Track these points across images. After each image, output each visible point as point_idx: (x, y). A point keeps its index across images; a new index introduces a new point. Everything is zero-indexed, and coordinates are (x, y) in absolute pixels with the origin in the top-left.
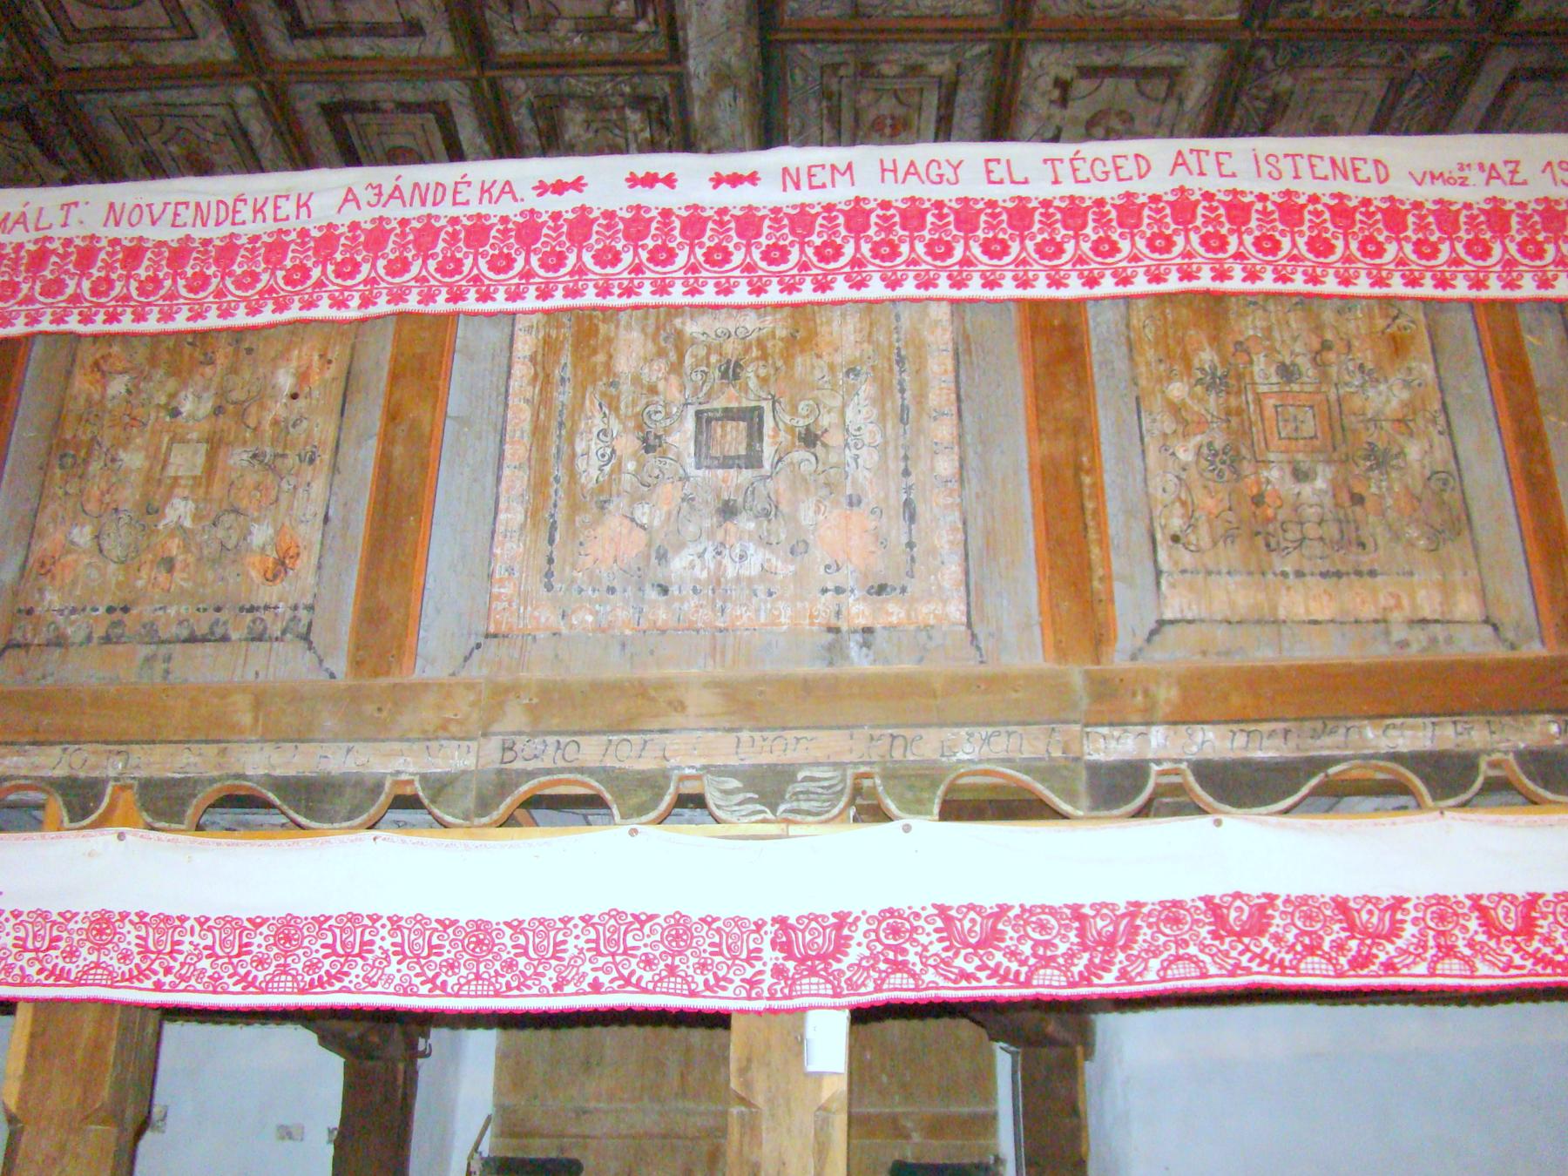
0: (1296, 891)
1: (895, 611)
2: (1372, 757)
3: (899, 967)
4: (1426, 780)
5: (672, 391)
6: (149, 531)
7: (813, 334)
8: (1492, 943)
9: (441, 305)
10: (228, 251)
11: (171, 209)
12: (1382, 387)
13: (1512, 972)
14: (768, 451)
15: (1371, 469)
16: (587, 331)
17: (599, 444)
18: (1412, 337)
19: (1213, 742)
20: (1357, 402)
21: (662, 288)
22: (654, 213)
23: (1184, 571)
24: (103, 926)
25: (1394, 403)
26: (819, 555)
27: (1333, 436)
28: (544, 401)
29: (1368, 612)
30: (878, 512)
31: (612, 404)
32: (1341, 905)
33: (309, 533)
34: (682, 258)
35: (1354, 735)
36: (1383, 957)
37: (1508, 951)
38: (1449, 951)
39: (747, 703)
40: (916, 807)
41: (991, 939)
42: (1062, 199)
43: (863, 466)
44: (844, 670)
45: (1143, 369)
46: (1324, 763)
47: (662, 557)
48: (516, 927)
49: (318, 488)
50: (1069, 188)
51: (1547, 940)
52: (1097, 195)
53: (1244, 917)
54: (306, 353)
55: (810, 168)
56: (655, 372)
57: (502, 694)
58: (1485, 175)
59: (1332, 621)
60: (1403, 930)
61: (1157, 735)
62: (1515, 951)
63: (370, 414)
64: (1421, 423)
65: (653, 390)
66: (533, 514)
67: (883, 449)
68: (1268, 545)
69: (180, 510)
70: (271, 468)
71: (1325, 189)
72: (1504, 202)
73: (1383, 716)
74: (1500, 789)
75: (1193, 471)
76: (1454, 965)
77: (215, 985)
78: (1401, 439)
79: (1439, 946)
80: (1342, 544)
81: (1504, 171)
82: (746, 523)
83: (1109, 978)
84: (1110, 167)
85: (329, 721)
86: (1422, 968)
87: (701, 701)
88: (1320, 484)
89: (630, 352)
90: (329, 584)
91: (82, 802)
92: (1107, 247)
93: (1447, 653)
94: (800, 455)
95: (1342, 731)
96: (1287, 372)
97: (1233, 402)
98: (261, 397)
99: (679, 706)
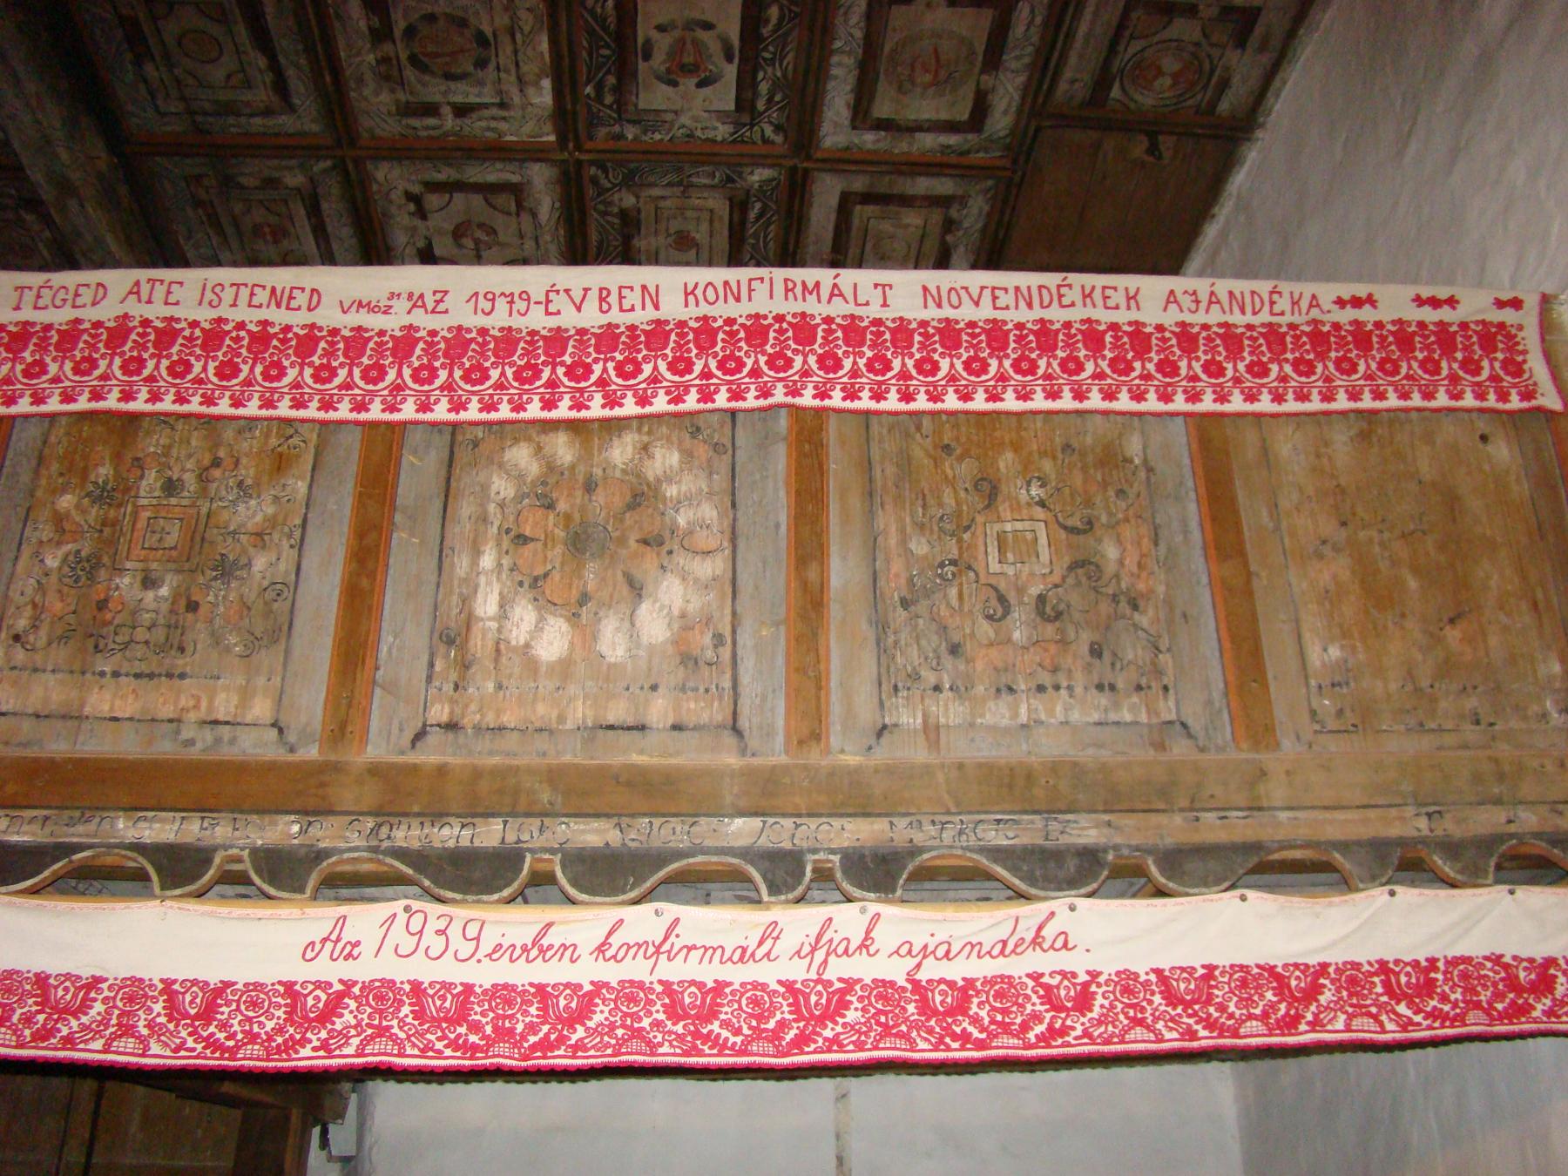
2: (117, 846)
4: (159, 871)
8: (171, 1026)
11: (987, 293)
12: (253, 502)
13: (183, 1053)
15: (215, 578)
18: (298, 456)
20: (225, 515)
22: (622, 329)
23: (14, 668)
25: (259, 518)
27: (191, 548)
29: (167, 711)
32: (41, 980)
35: (106, 825)
36: (65, 1031)
37: (184, 1034)
38: (127, 1030)
42: (794, 315)
45: (43, 482)
50: (27, 314)
51: (224, 1026)
52: (47, 321)
53: (321, 1005)
55: (620, 288)
58: (410, 304)
59: (131, 719)
60: (91, 1007)
62: (190, 1034)
64: (276, 536)
68: (96, 646)
71: (251, 317)
72: (1144, 325)
73: (137, 809)
74: (235, 883)
75: (54, 578)
76: (130, 1044)
78: (251, 550)
79: (119, 1025)
80: (163, 649)
83: (306, 1051)
84: (70, 297)
86: (98, 1044)
88: (164, 591)
92: (782, 362)
93: (228, 753)
95: (97, 820)
96: (171, 487)
97: (112, 513)
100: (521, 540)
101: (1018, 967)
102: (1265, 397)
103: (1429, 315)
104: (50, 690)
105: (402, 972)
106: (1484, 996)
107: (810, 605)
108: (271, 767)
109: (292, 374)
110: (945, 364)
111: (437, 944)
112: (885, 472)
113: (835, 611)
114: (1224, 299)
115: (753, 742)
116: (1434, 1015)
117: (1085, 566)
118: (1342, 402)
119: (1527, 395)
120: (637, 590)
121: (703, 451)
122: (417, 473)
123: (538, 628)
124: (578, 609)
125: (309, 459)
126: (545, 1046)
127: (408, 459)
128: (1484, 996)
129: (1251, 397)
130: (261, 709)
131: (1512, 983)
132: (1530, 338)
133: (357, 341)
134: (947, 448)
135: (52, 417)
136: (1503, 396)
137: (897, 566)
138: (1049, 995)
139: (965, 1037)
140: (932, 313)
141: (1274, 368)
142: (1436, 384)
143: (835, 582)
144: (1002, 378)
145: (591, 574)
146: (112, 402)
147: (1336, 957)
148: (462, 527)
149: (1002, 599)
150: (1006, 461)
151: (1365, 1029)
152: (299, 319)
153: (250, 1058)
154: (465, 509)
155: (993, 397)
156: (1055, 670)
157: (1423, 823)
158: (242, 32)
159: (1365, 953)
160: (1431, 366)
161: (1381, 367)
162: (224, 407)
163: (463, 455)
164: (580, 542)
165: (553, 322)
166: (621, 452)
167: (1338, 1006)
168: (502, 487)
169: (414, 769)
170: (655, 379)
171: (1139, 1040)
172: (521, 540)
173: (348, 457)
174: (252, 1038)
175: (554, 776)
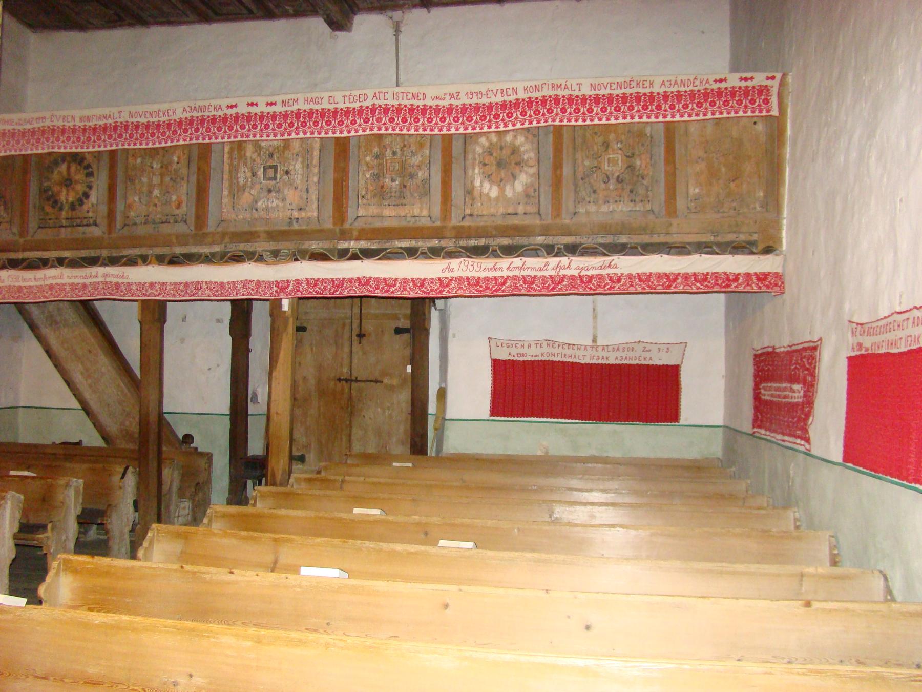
0: (376, 276)
1: (303, 215)
3: (298, 291)
5: (258, 160)
6: (150, 197)
7: (289, 145)
9: (207, 141)
10: (158, 126)
14: (278, 176)
16: (240, 145)
17: (243, 175)
19: (363, 244)
21: (255, 136)
24: (152, 285)
26: (288, 201)
28: (231, 165)
29: (403, 214)
30: (301, 191)
32: (385, 279)
33: (184, 198)
34: (259, 128)
38: (405, 290)
39: (273, 235)
40: (304, 258)
41: (316, 285)
43: (298, 179)
44: (292, 228)
46: (386, 249)
47: (256, 202)
48: (229, 283)
49: (185, 186)
50: (348, 105)
54: (179, 152)
56: (255, 156)
61: (352, 243)
63: (194, 169)
65: (254, 161)
66: (230, 192)
67: (303, 175)
69: (156, 192)
70: (175, 182)
71: (408, 103)
77: (174, 296)
80: (400, 197)
81: (455, 95)
82: (273, 194)
85: (191, 241)
87: (263, 235)
89: (249, 151)
90: (188, 209)
91: (145, 260)
93: (419, 224)
94: (285, 177)
96: (394, 153)
98: (171, 163)
99: (259, 237)
100: (485, 165)
101: (604, 272)
102: (686, 115)
103: (743, 84)
104: (373, 210)
105: (464, 275)
106: (720, 282)
107: (557, 183)
108: (429, 228)
109: (421, 120)
110: (595, 109)
111: (471, 268)
112: (579, 141)
113: (564, 182)
114: (679, 82)
115: (543, 217)
116: (706, 286)
117: (631, 167)
118: (709, 116)
119: (768, 111)
120: (514, 177)
121: (530, 137)
123: (490, 189)
124: (500, 183)
125: (428, 144)
126: (496, 290)
127: (454, 143)
130: (425, 213)
131: (728, 279)
132: (774, 91)
133: (437, 110)
134: (596, 133)
135: (360, 136)
137: (581, 169)
138: (611, 279)
139: (591, 288)
140: (593, 93)
141: (690, 106)
142: (739, 108)
143: (565, 173)
144: (611, 113)
146: (376, 131)
147: (683, 271)
149: (608, 178)
150: (612, 136)
151: (688, 289)
152: (421, 103)
154: (470, 156)
155: (608, 120)
156: (620, 196)
157: (712, 238)
159: (690, 271)
161: (724, 104)
162: (405, 132)
164: (500, 164)
165: (489, 101)
166: (509, 138)
167: (682, 283)
168: (479, 150)
169: (462, 227)
170: (517, 118)
171: (632, 290)
172: (485, 165)
173: (438, 142)
174: (432, 290)
175: (496, 228)
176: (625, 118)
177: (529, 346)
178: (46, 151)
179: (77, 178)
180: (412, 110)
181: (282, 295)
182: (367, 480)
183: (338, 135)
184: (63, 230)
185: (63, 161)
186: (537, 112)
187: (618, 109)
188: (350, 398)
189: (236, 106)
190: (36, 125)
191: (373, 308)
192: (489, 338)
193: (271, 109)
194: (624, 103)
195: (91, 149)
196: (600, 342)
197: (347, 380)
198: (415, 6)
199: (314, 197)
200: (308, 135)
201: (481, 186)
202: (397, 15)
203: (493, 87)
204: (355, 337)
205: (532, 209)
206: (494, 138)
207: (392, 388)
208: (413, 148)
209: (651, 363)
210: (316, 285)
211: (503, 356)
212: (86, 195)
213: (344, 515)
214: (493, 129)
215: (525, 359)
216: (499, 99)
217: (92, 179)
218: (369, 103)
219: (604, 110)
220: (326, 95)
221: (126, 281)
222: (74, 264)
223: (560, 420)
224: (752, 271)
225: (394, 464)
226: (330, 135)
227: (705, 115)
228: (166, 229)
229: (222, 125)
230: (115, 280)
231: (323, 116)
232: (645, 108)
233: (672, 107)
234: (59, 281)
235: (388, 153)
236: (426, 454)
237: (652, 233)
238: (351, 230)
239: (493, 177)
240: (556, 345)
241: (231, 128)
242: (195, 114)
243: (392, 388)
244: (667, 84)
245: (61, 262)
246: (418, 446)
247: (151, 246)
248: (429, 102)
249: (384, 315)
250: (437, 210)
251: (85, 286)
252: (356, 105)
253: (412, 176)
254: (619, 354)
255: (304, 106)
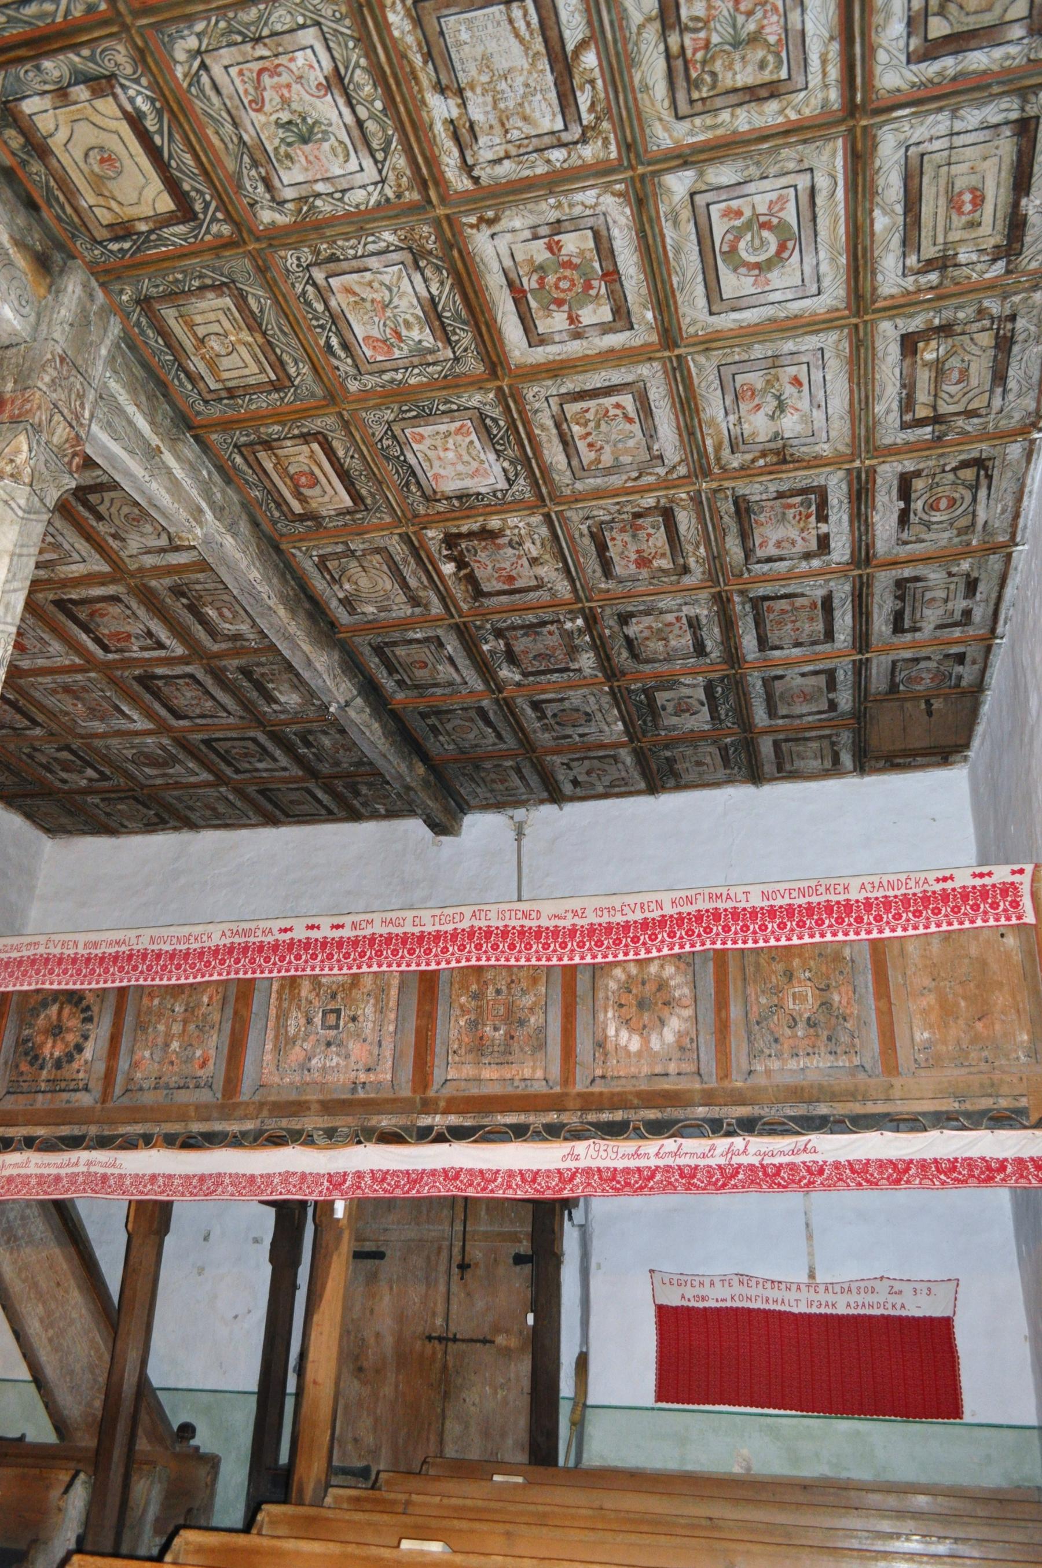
1: (372, 1077)
6: (166, 1052)
9: (249, 976)
16: (293, 982)
17: (295, 1022)
19: (453, 1120)
24: (153, 1178)
26: (353, 1059)
28: (279, 1007)
31: (299, 1007)
32: (481, 1171)
33: (212, 1053)
38: (509, 1187)
39: (328, 1107)
40: (369, 1140)
41: (384, 1179)
43: (368, 1027)
50: (437, 927)
54: (211, 990)
57: (262, 1105)
61: (438, 1118)
63: (229, 1012)
69: (175, 1045)
71: (516, 923)
80: (504, 1053)
82: (334, 1049)
87: (315, 1107)
89: (305, 989)
90: (215, 1069)
91: (148, 1141)
93: (531, 1090)
96: (498, 992)
98: (199, 1005)
100: (621, 1006)
101: (798, 1159)
103: (978, 882)
104: (468, 1071)
105: (594, 1164)
106: (976, 1173)
107: (722, 1029)
112: (750, 970)
113: (733, 1028)
118: (933, 928)
119: (1019, 918)
120: (662, 1022)
121: (682, 966)
122: (583, 982)
124: (643, 1031)
127: (579, 976)
128: (976, 1173)
129: (893, 930)
130: (539, 1074)
131: (989, 1168)
133: (556, 932)
136: (1008, 919)
138: (809, 1170)
140: (765, 904)
144: (792, 930)
145: (646, 1016)
147: (917, 1157)
148: (600, 1003)
152: (534, 924)
153: (549, 1195)
154: (601, 995)
158: (481, 724)
159: (929, 1155)
160: (975, 908)
162: (512, 962)
163: (598, 973)
164: (642, 1005)
166: (653, 969)
168: (613, 985)
169: (592, 1094)
172: (621, 1006)
175: (639, 1094)
176: (812, 936)
177: (712, 1284)
178: (33, 987)
179: (70, 1024)
180: (522, 933)
181: (335, 1195)
182: (446, 1501)
183: (423, 967)
184: (40, 1096)
185: (54, 1001)
186: (690, 933)
187: (801, 924)
188: (445, 1367)
189: (291, 929)
190: (25, 953)
191: (482, 1225)
192: (652, 1271)
193: (337, 934)
194: (810, 915)
195: (93, 986)
196: (819, 1279)
197: (440, 1339)
198: (542, 802)
199: (388, 1053)
200: (384, 968)
201: (617, 1035)
202: (520, 813)
203: (631, 900)
204: (455, 1270)
205: (688, 1067)
206: (633, 970)
207: (506, 1352)
208: (524, 984)
209: (904, 1313)
210: (384, 1179)
211: (674, 1300)
212: (79, 1049)
213: (386, 1553)
214: (631, 957)
215: (707, 1304)
216: (638, 916)
217: (89, 1026)
218: (465, 925)
219: (782, 926)
220: (409, 914)
221: (116, 1171)
222: (49, 1146)
223: (766, 1411)
224: (1025, 1155)
225: (497, 1478)
226: (413, 967)
227: (926, 927)
228: (183, 1097)
229: (271, 954)
230: (101, 1170)
231: (404, 942)
232: (840, 921)
233: (878, 918)
234: (23, 1171)
235: (491, 990)
236: (554, 1462)
237: (865, 1099)
238: (436, 1101)
239: (632, 1023)
240: (753, 1283)
241: (282, 959)
242: (237, 940)
243: (506, 1352)
244: (869, 887)
245: (29, 1143)
246: (541, 1450)
247: (158, 1121)
248: (545, 922)
249: (499, 1234)
250: (555, 1071)
251: (58, 1178)
252: (449, 928)
253: (522, 1023)
254: (852, 1298)
255: (379, 929)
